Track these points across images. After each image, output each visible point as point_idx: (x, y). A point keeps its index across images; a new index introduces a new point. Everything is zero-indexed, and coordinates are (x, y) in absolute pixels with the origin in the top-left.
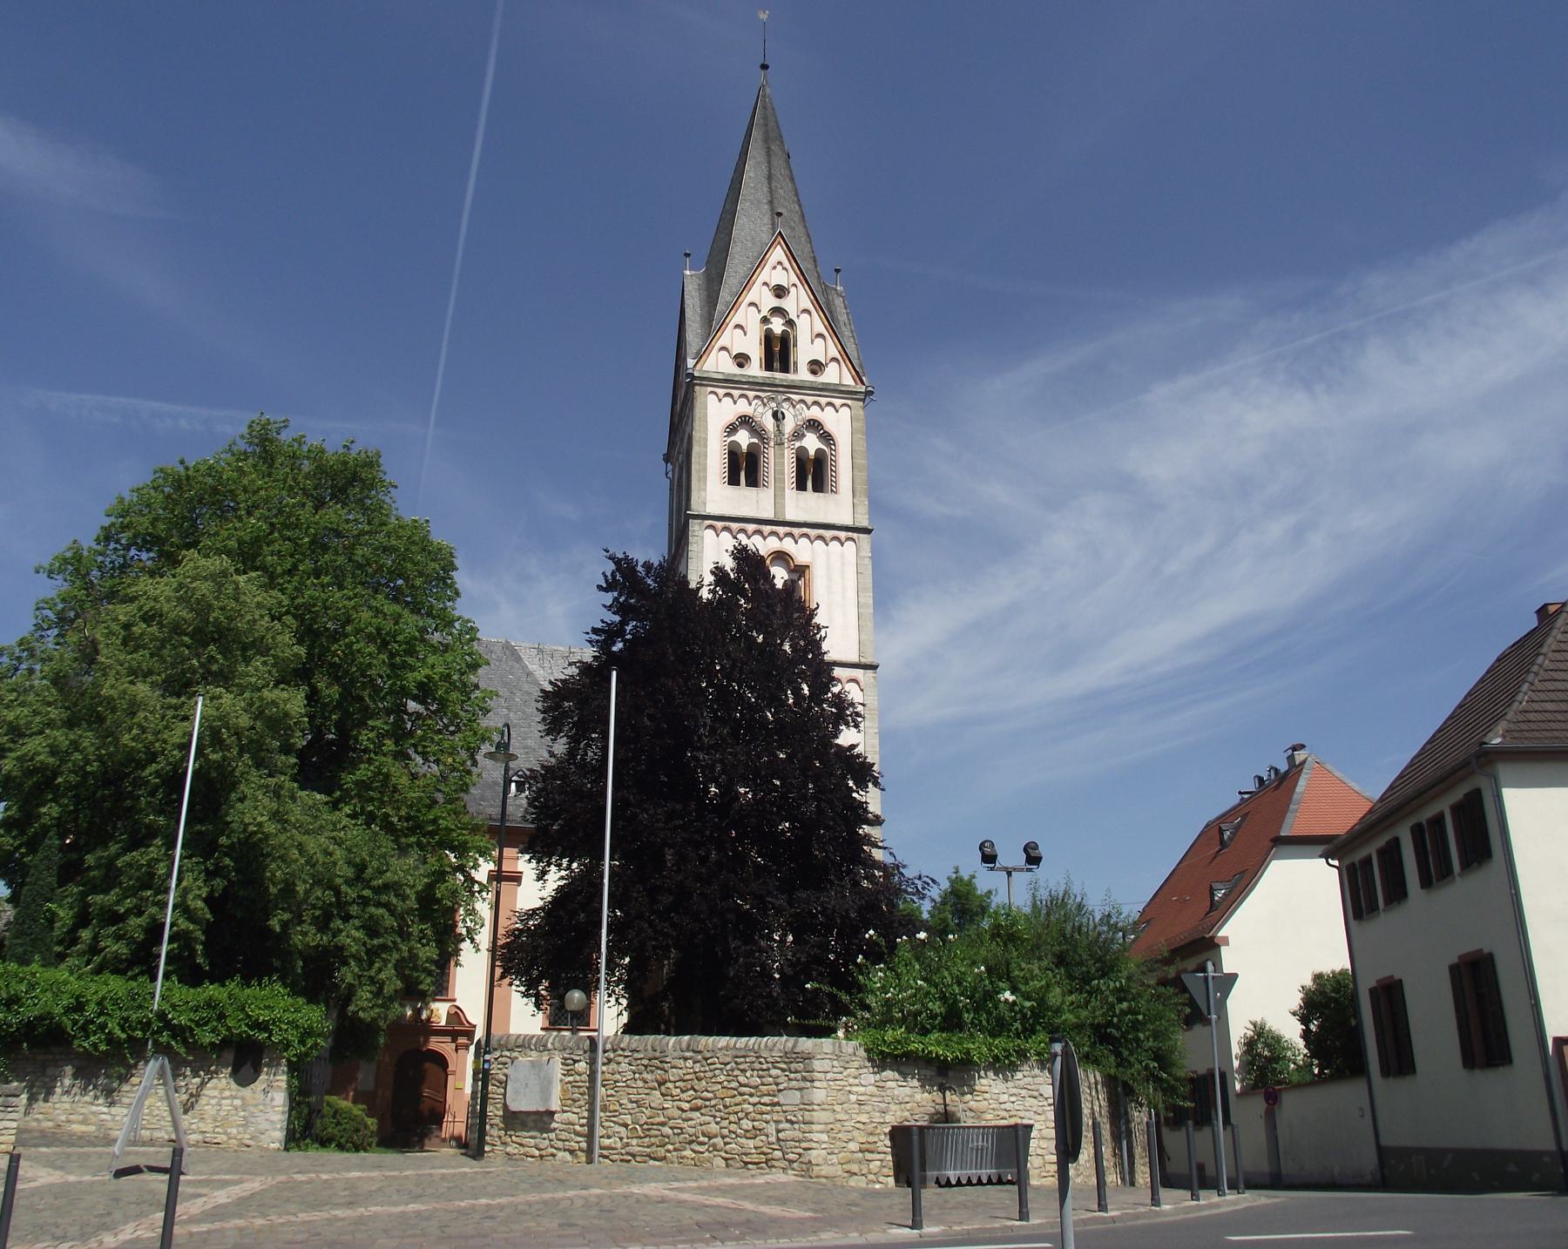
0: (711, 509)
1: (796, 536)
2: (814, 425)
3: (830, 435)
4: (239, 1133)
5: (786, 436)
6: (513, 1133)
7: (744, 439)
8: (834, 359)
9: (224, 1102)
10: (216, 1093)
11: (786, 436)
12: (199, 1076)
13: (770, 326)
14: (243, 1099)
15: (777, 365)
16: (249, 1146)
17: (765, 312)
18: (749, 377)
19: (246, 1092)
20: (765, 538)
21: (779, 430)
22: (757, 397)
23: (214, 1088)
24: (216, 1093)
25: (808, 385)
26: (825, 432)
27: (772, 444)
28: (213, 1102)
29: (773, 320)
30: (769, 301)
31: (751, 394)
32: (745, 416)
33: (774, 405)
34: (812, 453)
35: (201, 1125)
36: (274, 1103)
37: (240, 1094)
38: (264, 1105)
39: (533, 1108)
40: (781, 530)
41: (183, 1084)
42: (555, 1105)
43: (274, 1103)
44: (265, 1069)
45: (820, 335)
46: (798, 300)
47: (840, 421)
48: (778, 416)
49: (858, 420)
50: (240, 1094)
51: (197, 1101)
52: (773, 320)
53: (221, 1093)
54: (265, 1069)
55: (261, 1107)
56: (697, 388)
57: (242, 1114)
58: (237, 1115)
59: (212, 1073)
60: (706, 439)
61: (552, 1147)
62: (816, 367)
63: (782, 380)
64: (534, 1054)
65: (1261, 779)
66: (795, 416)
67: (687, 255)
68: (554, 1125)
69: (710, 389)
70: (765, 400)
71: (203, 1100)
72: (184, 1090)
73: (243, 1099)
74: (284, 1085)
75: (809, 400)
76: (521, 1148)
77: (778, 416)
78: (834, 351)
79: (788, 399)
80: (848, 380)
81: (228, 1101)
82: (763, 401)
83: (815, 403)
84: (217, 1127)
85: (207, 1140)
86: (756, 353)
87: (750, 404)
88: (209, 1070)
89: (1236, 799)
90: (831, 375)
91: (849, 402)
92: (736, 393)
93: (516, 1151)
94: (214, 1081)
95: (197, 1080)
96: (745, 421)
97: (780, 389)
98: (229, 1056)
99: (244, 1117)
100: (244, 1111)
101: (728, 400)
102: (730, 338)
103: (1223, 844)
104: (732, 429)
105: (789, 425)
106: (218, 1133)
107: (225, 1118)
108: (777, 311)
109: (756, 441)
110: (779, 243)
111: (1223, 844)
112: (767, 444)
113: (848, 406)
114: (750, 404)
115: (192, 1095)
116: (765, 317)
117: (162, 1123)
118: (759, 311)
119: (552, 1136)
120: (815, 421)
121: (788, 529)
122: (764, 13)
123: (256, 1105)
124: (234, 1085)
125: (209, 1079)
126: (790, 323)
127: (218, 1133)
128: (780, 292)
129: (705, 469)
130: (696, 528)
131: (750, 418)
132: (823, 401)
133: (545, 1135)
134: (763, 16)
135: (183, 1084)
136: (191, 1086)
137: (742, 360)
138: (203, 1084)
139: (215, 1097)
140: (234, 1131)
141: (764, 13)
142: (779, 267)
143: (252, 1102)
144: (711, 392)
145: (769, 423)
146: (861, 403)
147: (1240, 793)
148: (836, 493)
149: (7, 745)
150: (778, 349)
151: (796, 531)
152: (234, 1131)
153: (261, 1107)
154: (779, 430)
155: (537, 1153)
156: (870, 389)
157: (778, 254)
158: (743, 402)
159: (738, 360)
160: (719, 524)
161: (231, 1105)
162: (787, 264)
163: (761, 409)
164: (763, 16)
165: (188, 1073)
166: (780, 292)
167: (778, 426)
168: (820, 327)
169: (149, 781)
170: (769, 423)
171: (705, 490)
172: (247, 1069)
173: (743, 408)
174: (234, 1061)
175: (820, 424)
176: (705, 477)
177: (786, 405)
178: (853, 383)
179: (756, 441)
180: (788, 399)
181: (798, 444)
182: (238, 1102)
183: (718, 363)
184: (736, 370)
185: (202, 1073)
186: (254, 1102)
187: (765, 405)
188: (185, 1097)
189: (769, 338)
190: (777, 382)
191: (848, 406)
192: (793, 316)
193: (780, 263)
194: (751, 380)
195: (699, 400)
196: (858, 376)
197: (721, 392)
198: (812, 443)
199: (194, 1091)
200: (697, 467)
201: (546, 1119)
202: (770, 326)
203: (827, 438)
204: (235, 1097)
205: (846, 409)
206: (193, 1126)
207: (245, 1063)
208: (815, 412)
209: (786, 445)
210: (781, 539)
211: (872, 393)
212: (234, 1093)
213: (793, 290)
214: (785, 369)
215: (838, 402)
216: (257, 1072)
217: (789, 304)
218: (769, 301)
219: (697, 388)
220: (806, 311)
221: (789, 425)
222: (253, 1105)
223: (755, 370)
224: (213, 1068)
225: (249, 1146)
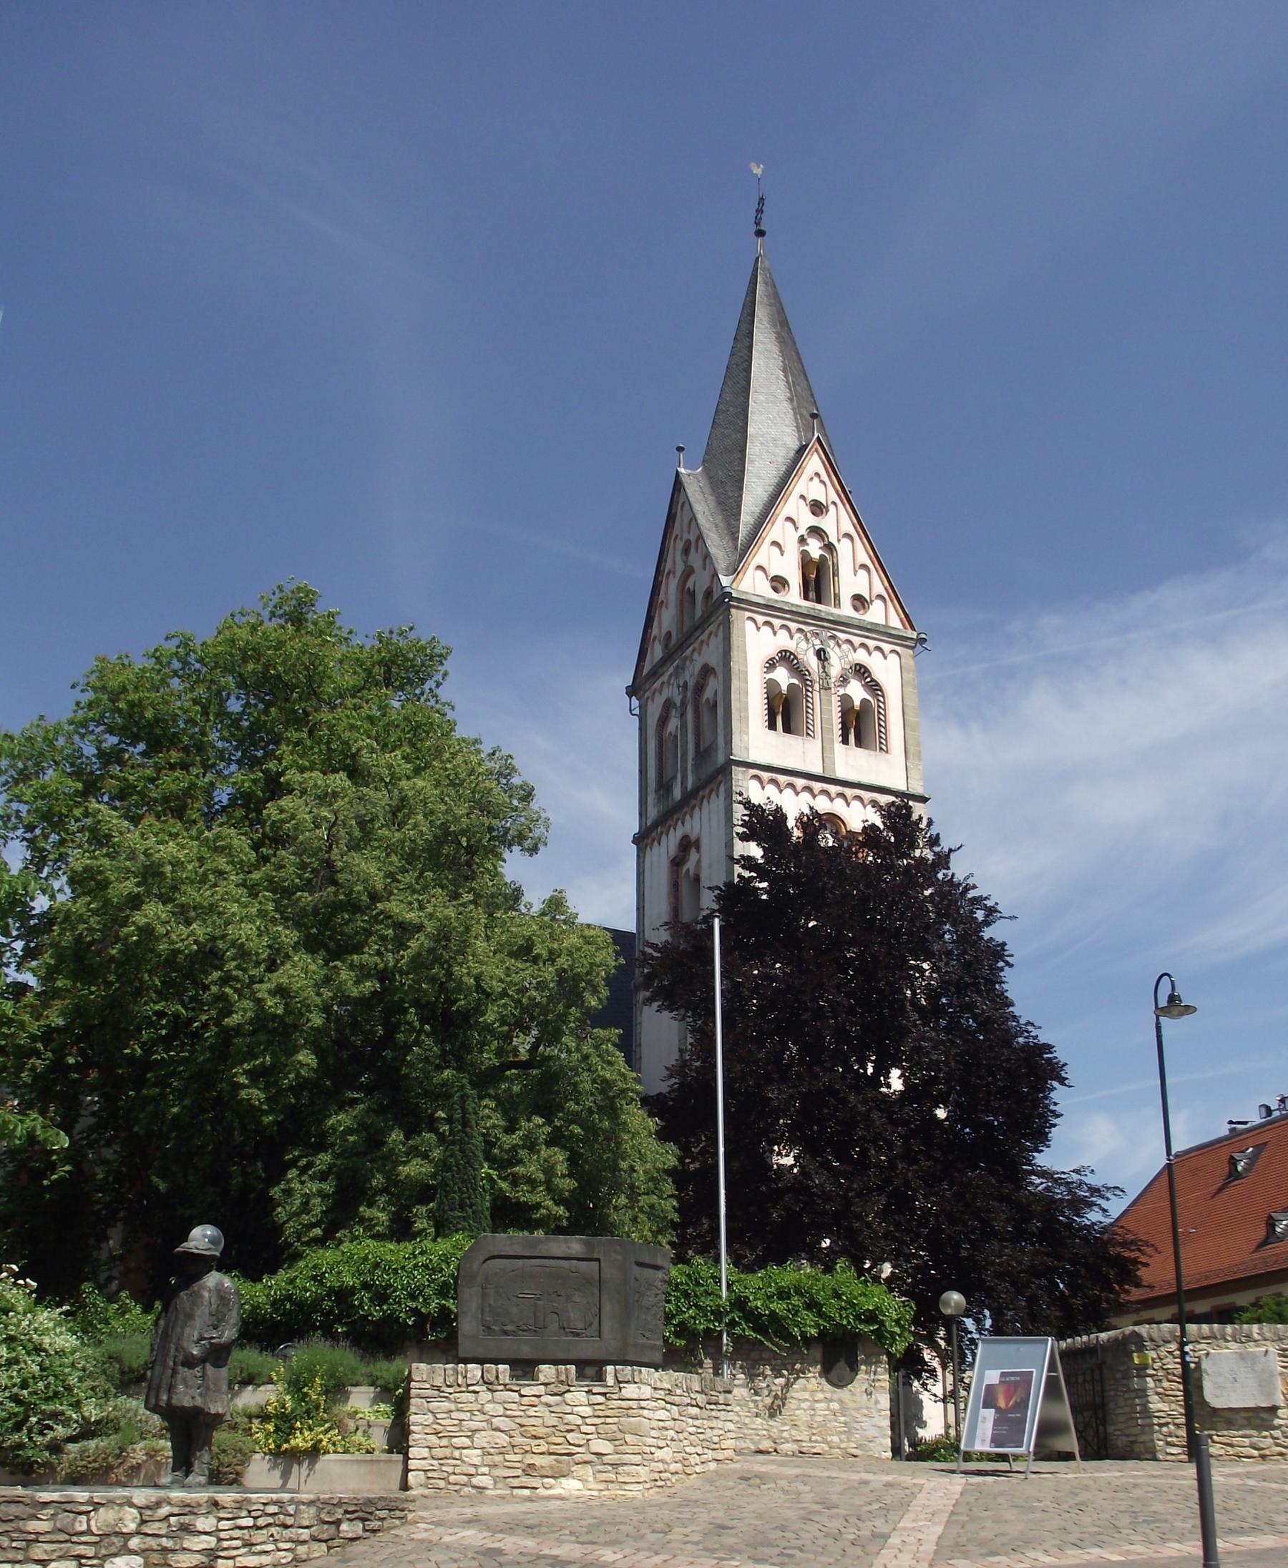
0: (754, 757)
1: (849, 798)
2: (861, 671)
3: (877, 684)
4: (841, 1441)
5: (833, 680)
6: (1214, 1432)
7: (783, 677)
8: (880, 597)
9: (817, 1405)
10: (807, 1395)
11: (833, 680)
12: (782, 1376)
13: (806, 548)
14: (841, 1402)
15: (812, 595)
16: (855, 1456)
17: (803, 531)
18: (793, 605)
19: (843, 1394)
20: (797, 794)
21: (824, 672)
22: (800, 630)
23: (805, 1389)
24: (807, 1395)
25: (856, 623)
26: (873, 680)
27: (817, 687)
28: (805, 1405)
29: (810, 540)
30: (806, 519)
31: (793, 626)
32: (786, 651)
33: (817, 642)
34: (857, 703)
35: (793, 1432)
36: (879, 1407)
37: (835, 1397)
38: (867, 1408)
39: (1251, 1404)
40: (833, 789)
41: (764, 1385)
42: (1280, 1400)
43: (879, 1407)
44: (863, 1367)
45: (864, 566)
46: (838, 522)
47: (887, 669)
48: (821, 655)
49: (908, 672)
50: (835, 1397)
51: (784, 1405)
52: (810, 540)
53: (812, 1396)
54: (863, 1367)
55: (865, 1411)
56: (733, 611)
57: (842, 1419)
58: (836, 1421)
59: (798, 1372)
60: (746, 673)
61: (1278, 1445)
62: (860, 602)
63: (828, 614)
64: (1233, 1345)
65: (1269, 1111)
66: (840, 658)
67: (680, 449)
68: (1277, 1422)
69: (748, 614)
70: (809, 635)
71: (791, 1404)
72: (766, 1392)
73: (841, 1402)
74: (887, 1385)
75: (857, 641)
76: (1229, 1449)
77: (821, 655)
78: (879, 588)
79: (833, 637)
80: (895, 622)
81: (823, 1405)
82: (806, 636)
83: (863, 645)
84: (814, 1434)
85: (804, 1450)
86: (795, 579)
87: (792, 637)
88: (793, 1369)
89: (1224, 1130)
90: (876, 614)
91: (898, 649)
92: (777, 623)
93: (1222, 1452)
94: (801, 1381)
95: (781, 1381)
96: (786, 658)
97: (826, 624)
98: (817, 1353)
99: (845, 1423)
100: (844, 1416)
101: (767, 629)
102: (763, 554)
103: (1233, 1175)
104: (771, 665)
105: (835, 670)
106: (816, 1442)
107: (823, 1424)
108: (816, 531)
109: (795, 681)
110: (817, 451)
111: (1233, 1175)
112: (812, 686)
113: (898, 653)
114: (792, 637)
115: (776, 1397)
116: (802, 536)
117: (746, 1431)
118: (796, 529)
119: (1277, 1433)
120: (861, 666)
121: (839, 789)
122: (759, 167)
123: (858, 1409)
124: (827, 1386)
125: (796, 1379)
126: (829, 547)
127: (816, 1442)
128: (817, 508)
129: (746, 709)
130: (740, 776)
131: (791, 653)
132: (871, 644)
133: (1265, 1433)
134: (757, 171)
135: (764, 1385)
136: (774, 1388)
137: (779, 583)
138: (788, 1385)
139: (807, 1400)
140: (836, 1439)
141: (759, 167)
142: (816, 479)
143: (851, 1405)
144: (750, 618)
145: (813, 663)
146: (911, 652)
147: (1231, 1122)
148: (887, 752)
149: (234, 973)
150: (813, 576)
151: (849, 792)
152: (836, 1439)
153: (865, 1411)
154: (824, 672)
155: (1255, 1453)
156: (923, 636)
157: (814, 463)
158: (783, 634)
159: (774, 584)
160: (766, 776)
161: (828, 1409)
162: (825, 477)
163: (803, 645)
164: (757, 171)
165: (769, 1372)
166: (817, 508)
167: (824, 667)
168: (863, 557)
169: (494, 1029)
170: (813, 663)
171: (747, 734)
172: (841, 1367)
173: (783, 641)
174: (824, 1355)
175: (867, 670)
176: (747, 718)
177: (832, 643)
178: (900, 626)
179: (795, 681)
180: (833, 637)
181: (842, 691)
182: (834, 1406)
183: (751, 584)
184: (773, 595)
185: (785, 1372)
186: (854, 1405)
187: (807, 640)
188: (768, 1400)
189: (806, 561)
190: (823, 615)
191: (898, 653)
192: (833, 539)
193: (817, 475)
194: (794, 609)
195: (735, 626)
196: (908, 620)
197: (760, 619)
198: (856, 691)
199: (779, 1393)
200: (738, 706)
201: (1265, 1415)
202: (806, 548)
203: (874, 687)
204: (831, 1400)
205: (893, 657)
206: (785, 1434)
207: (839, 1361)
208: (861, 656)
209: (833, 691)
210: (832, 800)
211: (925, 640)
212: (828, 1396)
213: (832, 508)
214: (819, 601)
215: (887, 647)
216: (854, 1370)
217: (827, 523)
218: (807, 519)
219: (733, 611)
220: (848, 535)
221: (835, 670)
222: (854, 1409)
223: (793, 596)
224: (798, 1366)
225: (855, 1456)
